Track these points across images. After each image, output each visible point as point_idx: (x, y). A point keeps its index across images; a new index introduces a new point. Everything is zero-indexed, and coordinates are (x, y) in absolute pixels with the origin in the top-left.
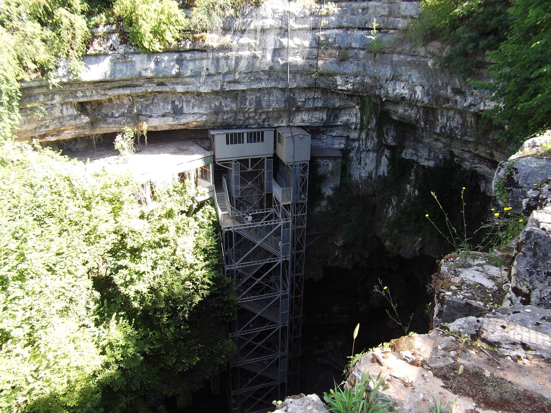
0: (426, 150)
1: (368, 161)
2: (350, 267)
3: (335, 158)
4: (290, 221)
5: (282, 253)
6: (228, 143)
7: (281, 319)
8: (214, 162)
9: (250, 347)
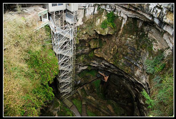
0: (109, 6)
1: (91, 9)
2: (87, 39)
3: (83, 9)
4: (73, 28)
5: (71, 37)
6: (52, 6)
7: (71, 55)
8: (48, 13)
9: (63, 64)
